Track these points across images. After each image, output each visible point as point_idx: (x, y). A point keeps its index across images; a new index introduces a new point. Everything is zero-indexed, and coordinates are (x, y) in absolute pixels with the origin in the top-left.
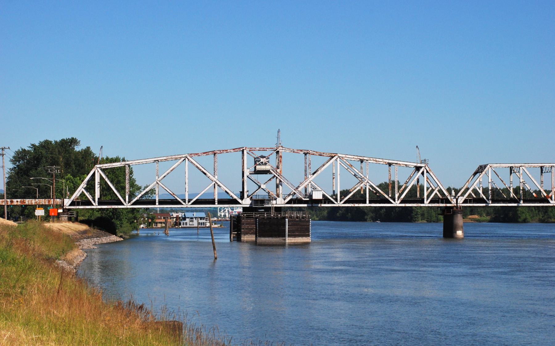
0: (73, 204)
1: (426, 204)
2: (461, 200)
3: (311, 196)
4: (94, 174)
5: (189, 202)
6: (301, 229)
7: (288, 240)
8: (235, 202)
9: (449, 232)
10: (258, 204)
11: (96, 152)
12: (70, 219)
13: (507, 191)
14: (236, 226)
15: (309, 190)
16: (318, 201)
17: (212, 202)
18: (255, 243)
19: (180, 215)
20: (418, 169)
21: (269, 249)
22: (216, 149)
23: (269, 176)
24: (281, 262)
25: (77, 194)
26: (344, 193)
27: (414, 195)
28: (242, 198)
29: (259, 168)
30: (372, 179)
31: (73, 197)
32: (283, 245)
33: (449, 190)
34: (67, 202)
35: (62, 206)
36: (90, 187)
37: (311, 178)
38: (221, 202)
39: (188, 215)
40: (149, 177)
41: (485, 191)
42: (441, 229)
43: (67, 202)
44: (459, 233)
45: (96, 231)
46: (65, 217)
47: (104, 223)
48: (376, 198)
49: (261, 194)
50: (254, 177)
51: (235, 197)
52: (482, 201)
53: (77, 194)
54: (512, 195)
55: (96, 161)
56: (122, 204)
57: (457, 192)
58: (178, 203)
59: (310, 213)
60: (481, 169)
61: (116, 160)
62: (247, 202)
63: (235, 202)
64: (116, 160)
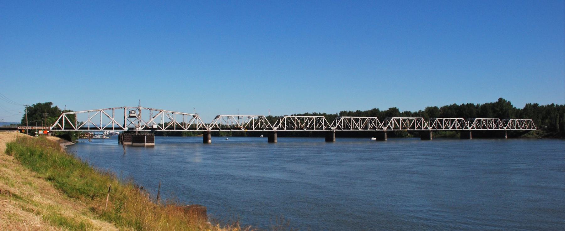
0: (53, 129)
1: (198, 130)
2: (210, 128)
3: (152, 126)
4: (62, 117)
5: (165, 126)
6: (151, 140)
7: (146, 144)
8: (121, 129)
9: (206, 141)
10: (131, 129)
11: (61, 108)
12: (52, 135)
13: (226, 126)
14: (121, 139)
15: (152, 124)
16: (156, 129)
17: (87, 129)
18: (132, 146)
19: (93, 133)
20: (194, 116)
21: (7, 132)
22: (113, 107)
23: (135, 118)
24: (141, 152)
25: (55, 124)
26: (166, 124)
27: (193, 127)
28: (124, 126)
29: (131, 115)
30: (177, 120)
31: (54, 126)
32: (144, 146)
33: (206, 125)
34: (51, 128)
35: (49, 130)
36: (61, 122)
37: (152, 119)
38: (115, 129)
39: (96, 133)
40: (86, 117)
41: (219, 125)
42: (202, 139)
43: (51, 128)
44: (210, 141)
45: (63, 140)
46: (50, 134)
47: (66, 137)
48: (178, 127)
49: (132, 126)
50: (129, 119)
51: (121, 127)
52: (218, 129)
53: (55, 124)
54: (218, 126)
55: (63, 112)
56: (61, 129)
57: (209, 125)
58: (98, 129)
59: (154, 134)
60: (217, 117)
61: (69, 111)
62: (126, 129)
63: (121, 129)
64: (69, 111)
